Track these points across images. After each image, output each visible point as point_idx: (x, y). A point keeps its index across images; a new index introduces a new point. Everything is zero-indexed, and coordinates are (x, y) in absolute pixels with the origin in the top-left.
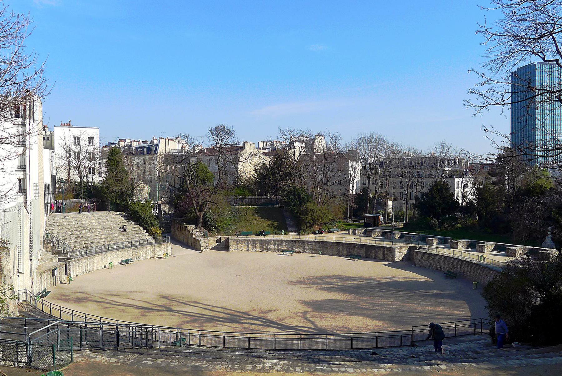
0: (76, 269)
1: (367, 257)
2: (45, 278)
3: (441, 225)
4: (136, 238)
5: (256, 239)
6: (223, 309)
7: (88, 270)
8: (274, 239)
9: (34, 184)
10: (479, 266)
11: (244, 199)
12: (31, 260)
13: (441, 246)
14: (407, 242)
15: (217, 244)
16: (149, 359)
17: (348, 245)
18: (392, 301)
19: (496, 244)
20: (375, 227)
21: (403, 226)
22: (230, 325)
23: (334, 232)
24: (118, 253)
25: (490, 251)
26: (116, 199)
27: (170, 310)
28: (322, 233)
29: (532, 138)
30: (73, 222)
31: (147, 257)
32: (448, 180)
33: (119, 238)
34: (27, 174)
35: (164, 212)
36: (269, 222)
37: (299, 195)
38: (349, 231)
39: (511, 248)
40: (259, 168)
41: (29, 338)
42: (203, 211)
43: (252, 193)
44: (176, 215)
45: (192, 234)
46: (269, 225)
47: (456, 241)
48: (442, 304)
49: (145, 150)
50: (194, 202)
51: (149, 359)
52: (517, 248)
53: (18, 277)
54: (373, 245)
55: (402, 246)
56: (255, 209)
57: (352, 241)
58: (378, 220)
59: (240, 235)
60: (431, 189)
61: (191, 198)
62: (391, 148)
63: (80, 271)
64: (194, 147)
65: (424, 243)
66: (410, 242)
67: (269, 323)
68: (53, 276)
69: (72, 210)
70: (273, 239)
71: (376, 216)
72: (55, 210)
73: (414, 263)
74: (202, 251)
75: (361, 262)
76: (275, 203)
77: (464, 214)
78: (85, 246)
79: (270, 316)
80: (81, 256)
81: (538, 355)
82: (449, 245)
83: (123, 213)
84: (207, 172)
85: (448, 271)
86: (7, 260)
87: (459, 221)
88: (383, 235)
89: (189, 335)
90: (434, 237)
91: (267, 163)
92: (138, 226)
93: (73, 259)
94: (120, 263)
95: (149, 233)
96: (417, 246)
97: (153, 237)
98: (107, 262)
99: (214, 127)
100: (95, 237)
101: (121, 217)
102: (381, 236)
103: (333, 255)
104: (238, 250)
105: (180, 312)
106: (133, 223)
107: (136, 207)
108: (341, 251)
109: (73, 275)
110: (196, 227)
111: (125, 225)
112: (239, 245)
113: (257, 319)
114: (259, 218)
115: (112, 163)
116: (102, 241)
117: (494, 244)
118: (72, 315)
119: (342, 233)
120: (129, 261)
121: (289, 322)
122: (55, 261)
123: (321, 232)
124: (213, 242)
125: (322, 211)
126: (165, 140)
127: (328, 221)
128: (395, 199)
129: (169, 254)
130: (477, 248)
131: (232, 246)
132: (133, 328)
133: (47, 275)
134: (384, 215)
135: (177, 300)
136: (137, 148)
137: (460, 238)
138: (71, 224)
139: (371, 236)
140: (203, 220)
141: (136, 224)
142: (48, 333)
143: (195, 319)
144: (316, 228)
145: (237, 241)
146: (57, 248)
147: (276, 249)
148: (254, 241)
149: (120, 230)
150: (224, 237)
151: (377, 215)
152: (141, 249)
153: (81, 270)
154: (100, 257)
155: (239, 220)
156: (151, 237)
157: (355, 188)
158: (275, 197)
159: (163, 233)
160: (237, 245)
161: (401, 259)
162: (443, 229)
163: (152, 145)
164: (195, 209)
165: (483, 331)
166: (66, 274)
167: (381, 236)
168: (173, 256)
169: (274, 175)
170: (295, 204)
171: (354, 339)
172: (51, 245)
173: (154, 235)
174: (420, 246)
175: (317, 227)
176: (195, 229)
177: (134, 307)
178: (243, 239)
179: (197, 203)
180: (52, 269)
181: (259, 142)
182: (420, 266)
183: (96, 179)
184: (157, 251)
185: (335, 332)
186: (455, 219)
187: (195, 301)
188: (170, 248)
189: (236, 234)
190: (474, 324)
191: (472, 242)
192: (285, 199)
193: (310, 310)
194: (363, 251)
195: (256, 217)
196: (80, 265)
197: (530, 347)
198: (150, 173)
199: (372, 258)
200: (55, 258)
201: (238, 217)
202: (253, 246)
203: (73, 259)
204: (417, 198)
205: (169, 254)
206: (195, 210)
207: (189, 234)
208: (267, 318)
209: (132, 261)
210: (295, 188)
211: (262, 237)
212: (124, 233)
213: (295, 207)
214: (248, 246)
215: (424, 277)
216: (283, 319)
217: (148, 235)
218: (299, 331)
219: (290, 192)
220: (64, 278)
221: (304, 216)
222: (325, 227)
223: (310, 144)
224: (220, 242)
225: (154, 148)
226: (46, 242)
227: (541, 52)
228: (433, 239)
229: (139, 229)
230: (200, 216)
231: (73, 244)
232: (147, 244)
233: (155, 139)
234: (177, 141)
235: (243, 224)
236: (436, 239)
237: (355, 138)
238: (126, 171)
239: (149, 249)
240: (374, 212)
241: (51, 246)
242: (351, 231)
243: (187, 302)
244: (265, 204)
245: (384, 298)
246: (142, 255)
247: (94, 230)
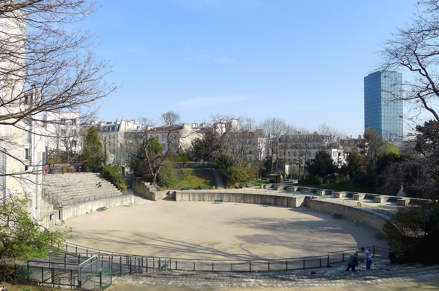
0: (67, 214)
1: (276, 204)
2: (45, 221)
3: (325, 182)
4: (108, 192)
5: (196, 192)
6: (181, 243)
7: (75, 215)
8: (209, 192)
9: (37, 153)
10: (358, 209)
11: (185, 163)
12: (36, 208)
13: (328, 196)
14: (303, 193)
15: (167, 195)
16: (163, 281)
17: (261, 196)
18: (300, 235)
19: (366, 194)
20: (278, 183)
21: (297, 183)
22: (188, 254)
23: (250, 187)
24: (96, 203)
25: (362, 200)
26: (93, 164)
27: (143, 244)
28: (241, 188)
29: (380, 122)
30: (62, 180)
31: (117, 206)
32: (328, 150)
33: (96, 192)
34: (32, 145)
35: (127, 173)
36: (203, 180)
37: (225, 161)
38: (261, 186)
39: (378, 197)
40: (195, 142)
41: (80, 267)
42: (156, 172)
43: (190, 159)
44: (135, 174)
45: (148, 189)
46: (204, 182)
47: (338, 193)
48: (336, 237)
49: (111, 128)
50: (150, 166)
51: (163, 281)
52: (381, 197)
54: (280, 195)
55: (300, 196)
56: (194, 171)
57: (264, 193)
58: (280, 179)
59: (183, 189)
60: (317, 156)
61: (148, 163)
62: (288, 129)
63: (69, 216)
64: (147, 127)
65: (315, 194)
66: (305, 194)
67: (216, 252)
68: (50, 220)
69: (62, 171)
70: (207, 192)
71: (279, 176)
72: (48, 171)
73: (309, 208)
74: (156, 200)
75: (271, 208)
76: (207, 167)
77: (340, 174)
78: (72, 198)
79: (217, 247)
80: (69, 204)
81: (437, 271)
82: (333, 196)
83: (98, 174)
84: (158, 144)
85: (335, 214)
86: (30, 208)
87: (337, 178)
88: (285, 188)
89: (170, 263)
90: (322, 190)
91: (201, 139)
92: (110, 183)
93: (64, 207)
94: (97, 210)
95: (118, 188)
96: (311, 196)
97: (121, 191)
98: (88, 209)
99: (165, 113)
100: (79, 191)
101: (97, 176)
102: (284, 189)
103: (251, 203)
104: (182, 200)
105: (150, 245)
106: (106, 181)
107: (108, 169)
108: (256, 200)
109: (64, 218)
110: (151, 184)
111: (100, 183)
112: (183, 196)
113: (207, 249)
114: (196, 177)
115: (91, 138)
116: (84, 194)
118: (76, 249)
119: (256, 188)
120: (104, 208)
121: (231, 251)
122: (51, 209)
123: (241, 187)
124: (163, 194)
125: (242, 172)
126: (125, 121)
127: (246, 179)
128: (290, 164)
129: (133, 203)
130: (353, 197)
131: (178, 197)
132: (139, 258)
133: (46, 219)
134: (283, 175)
135: (146, 237)
136: (105, 127)
137: (341, 190)
138: (61, 182)
139: (277, 190)
140: (156, 178)
141: (108, 182)
142: (91, 263)
143: (163, 250)
144: (237, 184)
145: (182, 193)
146: (52, 199)
148: (194, 194)
149: (96, 186)
150: (171, 191)
151: (279, 175)
152: (113, 200)
153: (70, 215)
154: (84, 206)
155: (182, 179)
156: (119, 191)
157: (263, 156)
158: (207, 162)
159: (128, 188)
160: (182, 197)
161: (300, 206)
162: (326, 184)
163: (115, 125)
164: (151, 171)
165: (375, 255)
166: (59, 218)
167: (284, 189)
168: (135, 205)
169: (206, 146)
170: (223, 167)
171: (305, 261)
172: (48, 197)
173: (121, 189)
174: (312, 196)
175: (237, 183)
176: (150, 185)
177: (117, 242)
178: (186, 192)
179: (152, 167)
180: (50, 215)
181: (192, 124)
182: (314, 210)
183: (78, 149)
184: (124, 201)
185: (266, 258)
186: (335, 177)
187: (159, 237)
188: (133, 199)
189: (180, 189)
190: (320, 260)
192: (215, 164)
193: (244, 242)
194: (273, 201)
195: (194, 177)
196: (69, 212)
197: (423, 265)
198: (114, 145)
199: (279, 205)
200: (51, 206)
201: (181, 175)
203: (64, 207)
204: (307, 163)
205: (133, 203)
206: (151, 171)
207: (147, 189)
208: (215, 248)
209: (106, 209)
210: (221, 156)
211: (199, 190)
212: (100, 188)
213: (222, 169)
214: (189, 197)
215: (318, 218)
216: (226, 249)
217: (117, 189)
218: (239, 257)
219: (219, 159)
220: (58, 221)
221: (229, 175)
222: (243, 183)
223: (229, 125)
224: (169, 195)
225: (117, 127)
226: (44, 195)
227: (409, 64)
228: (322, 192)
229: (110, 185)
230: (155, 176)
231: (63, 196)
232: (117, 196)
233: (117, 121)
234: (133, 122)
235: (185, 182)
236: (324, 191)
237: (263, 121)
238: (100, 143)
239: (119, 200)
240: (276, 172)
241: (48, 198)
242: (262, 186)
243: (154, 238)
244: (200, 167)
245: (294, 232)
246: (113, 204)
247: (78, 186)
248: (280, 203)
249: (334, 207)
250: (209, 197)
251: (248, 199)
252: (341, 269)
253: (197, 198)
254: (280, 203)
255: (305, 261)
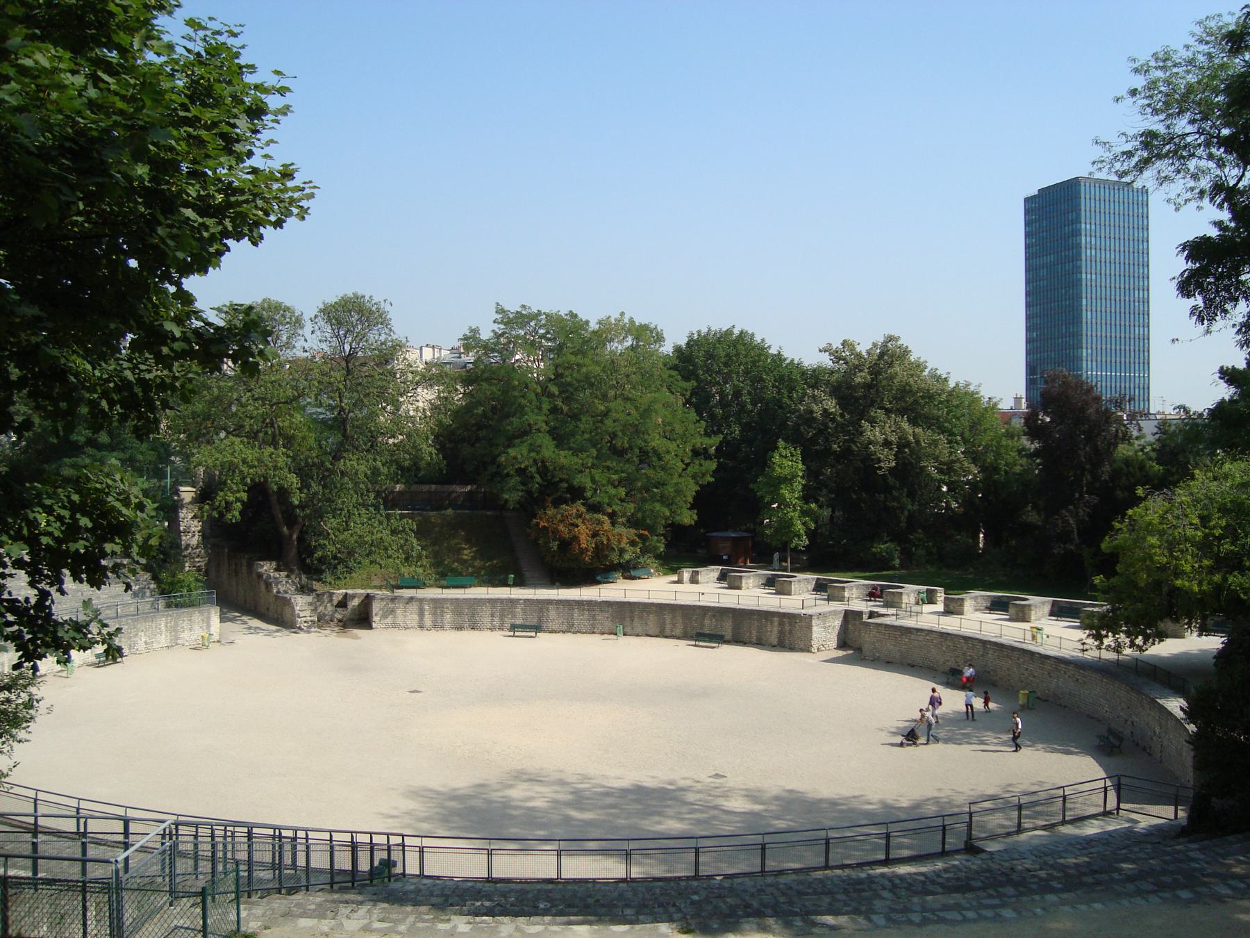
1: (738, 640)
53: (214, 19)
117: (1048, 602)
147: (497, 622)
148: (436, 603)
190: (824, 842)
191: (995, 597)
202: (434, 614)
214: (421, 614)
239: (163, 625)
248: (754, 633)
249: (948, 647)
250: (492, 615)
251: (637, 622)
252: (956, 863)
253: (448, 617)
254: (754, 633)
255: (767, 846)
